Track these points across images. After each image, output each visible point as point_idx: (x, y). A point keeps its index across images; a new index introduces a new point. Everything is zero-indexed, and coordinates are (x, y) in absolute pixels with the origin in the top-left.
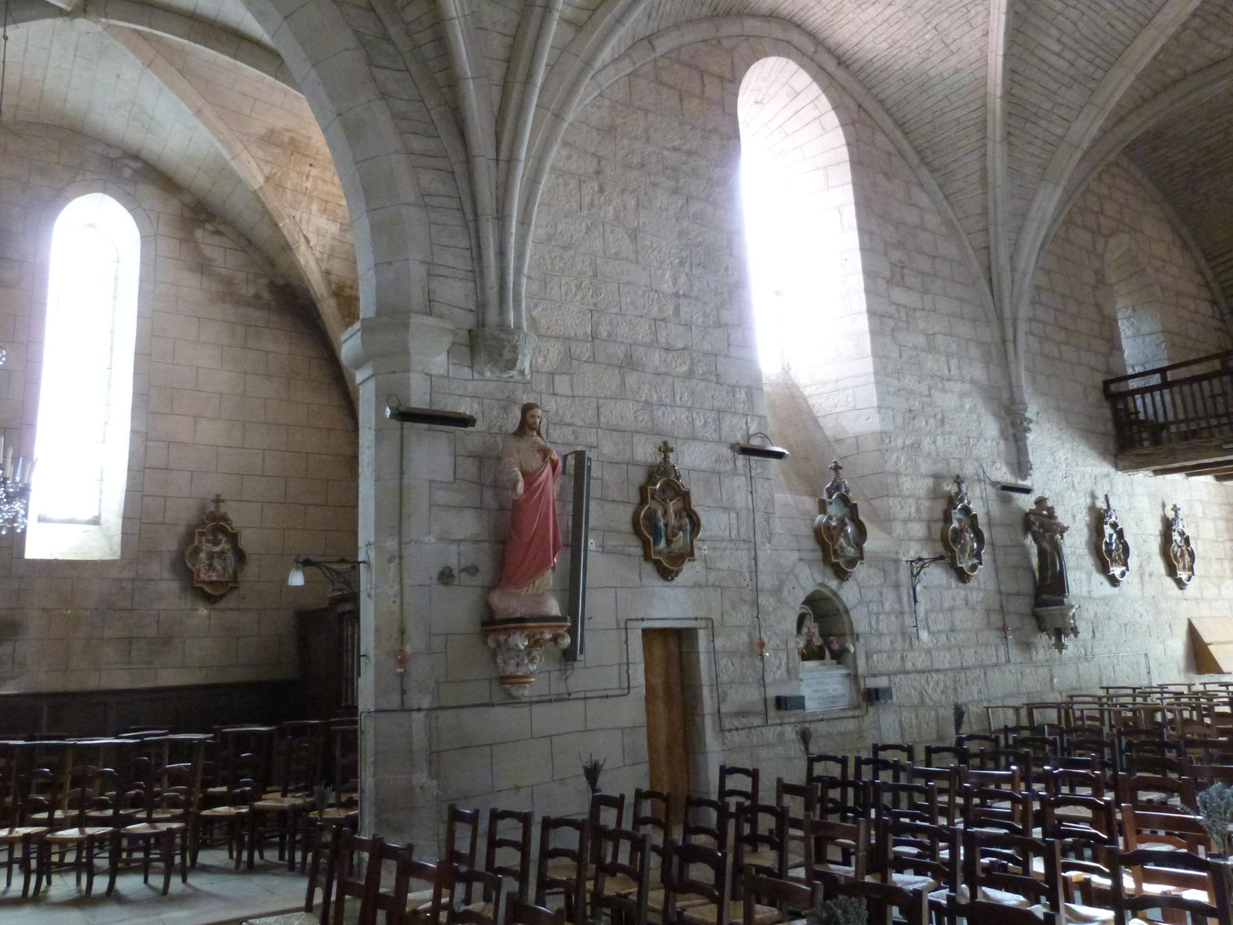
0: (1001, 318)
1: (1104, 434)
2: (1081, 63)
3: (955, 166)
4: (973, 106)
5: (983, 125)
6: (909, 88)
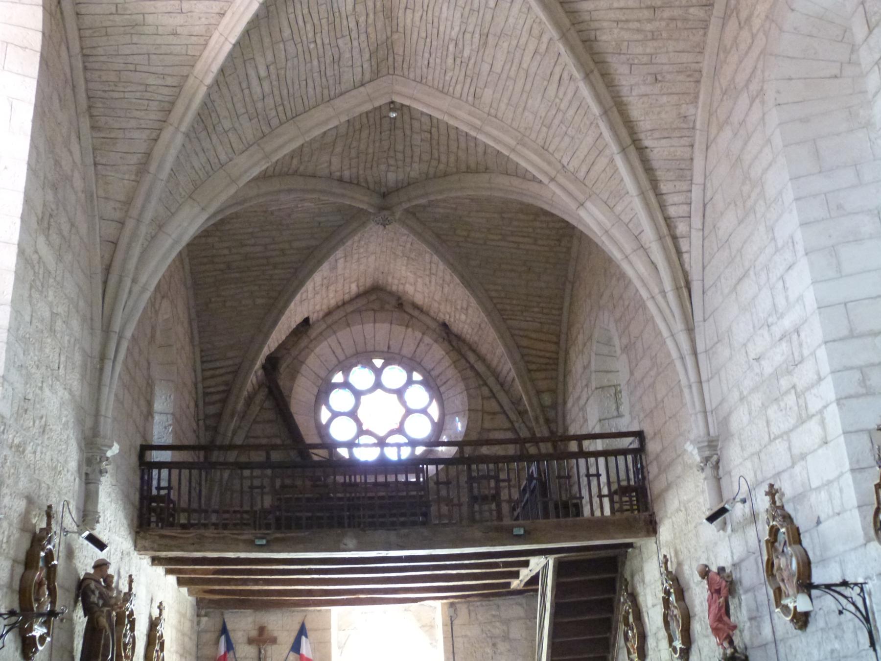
0: (107, 330)
1: (133, 504)
2: (270, 101)
3: (120, 134)
4: (170, 81)
5: (168, 109)
6: (117, 18)
